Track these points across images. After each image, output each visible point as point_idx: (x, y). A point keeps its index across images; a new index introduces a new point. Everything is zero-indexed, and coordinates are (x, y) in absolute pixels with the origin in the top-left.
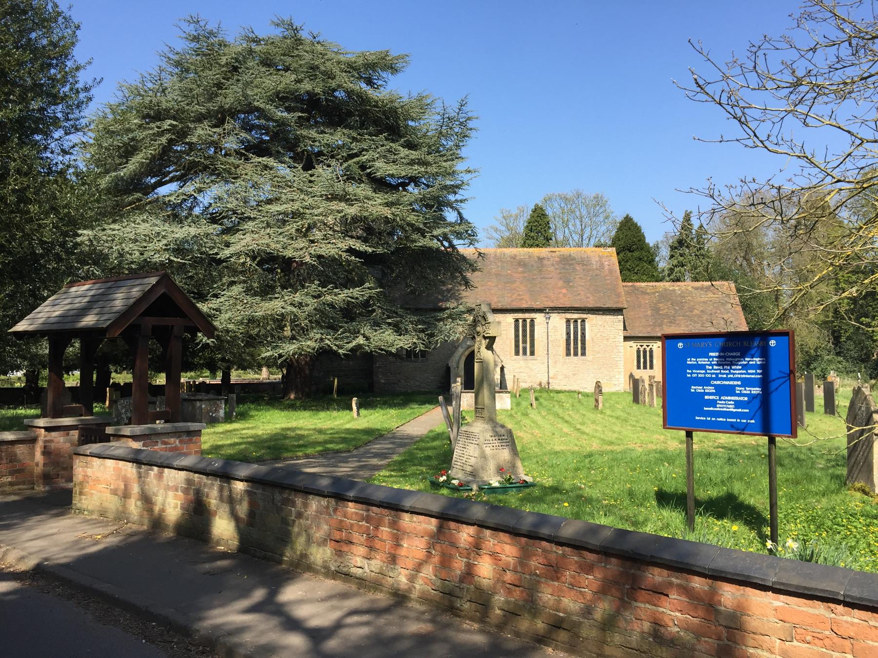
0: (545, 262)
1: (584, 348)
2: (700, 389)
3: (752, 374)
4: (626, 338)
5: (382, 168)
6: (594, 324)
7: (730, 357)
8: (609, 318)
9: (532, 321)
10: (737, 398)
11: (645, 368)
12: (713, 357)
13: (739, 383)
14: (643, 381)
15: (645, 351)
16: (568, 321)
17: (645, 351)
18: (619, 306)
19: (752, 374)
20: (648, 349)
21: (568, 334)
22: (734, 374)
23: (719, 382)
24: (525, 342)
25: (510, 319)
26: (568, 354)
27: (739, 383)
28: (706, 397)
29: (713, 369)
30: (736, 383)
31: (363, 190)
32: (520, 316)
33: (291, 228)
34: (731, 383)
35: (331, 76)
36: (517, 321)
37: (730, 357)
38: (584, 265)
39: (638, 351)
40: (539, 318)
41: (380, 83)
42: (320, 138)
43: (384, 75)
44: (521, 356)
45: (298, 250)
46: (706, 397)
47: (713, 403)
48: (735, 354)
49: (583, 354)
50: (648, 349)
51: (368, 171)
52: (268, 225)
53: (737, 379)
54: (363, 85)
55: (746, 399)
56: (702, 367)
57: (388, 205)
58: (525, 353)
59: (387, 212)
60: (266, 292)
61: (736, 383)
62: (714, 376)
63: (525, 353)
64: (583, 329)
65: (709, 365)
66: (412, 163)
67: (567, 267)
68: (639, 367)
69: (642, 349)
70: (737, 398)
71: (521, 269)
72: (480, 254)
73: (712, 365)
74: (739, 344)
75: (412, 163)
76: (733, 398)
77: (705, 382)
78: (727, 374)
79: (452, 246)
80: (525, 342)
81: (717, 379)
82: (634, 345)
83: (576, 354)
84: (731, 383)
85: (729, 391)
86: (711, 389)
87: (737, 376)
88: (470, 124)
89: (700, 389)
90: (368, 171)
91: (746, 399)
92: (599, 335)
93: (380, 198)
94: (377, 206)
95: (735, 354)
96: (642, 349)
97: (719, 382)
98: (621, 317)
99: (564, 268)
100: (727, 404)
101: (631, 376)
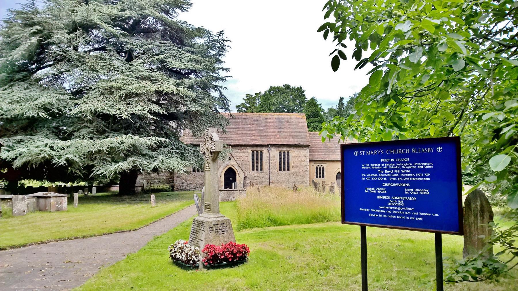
0: (268, 120)
1: (288, 167)
2: (373, 190)
3: (420, 177)
4: (310, 161)
5: (175, 64)
6: (294, 154)
7: (399, 162)
8: (301, 150)
9: (261, 153)
10: (406, 198)
11: (320, 177)
12: (385, 163)
13: (408, 185)
14: (319, 184)
15: (320, 168)
16: (280, 153)
17: (320, 168)
18: (307, 144)
19: (420, 177)
20: (322, 167)
21: (280, 159)
22: (403, 177)
23: (389, 185)
24: (257, 163)
25: (249, 151)
26: (280, 170)
27: (408, 185)
28: (378, 197)
29: (384, 173)
30: (405, 185)
31: (160, 75)
32: (255, 149)
33: (116, 95)
34: (401, 185)
35: (143, 8)
36: (253, 152)
37: (399, 162)
38: (289, 122)
39: (317, 168)
40: (265, 151)
41: (174, 14)
42: (135, 42)
43: (177, 10)
44: (255, 171)
45: (124, 111)
46: (378, 197)
47: (385, 202)
48: (404, 160)
49: (288, 170)
50: (322, 167)
51: (164, 64)
52: (102, 94)
53: (406, 182)
54: (165, 15)
55: (414, 199)
56: (375, 171)
57: (178, 85)
58: (257, 169)
59: (175, 89)
60: (102, 133)
61: (405, 185)
62: (385, 179)
63: (257, 169)
64: (288, 156)
65: (381, 170)
66: (190, 60)
67: (280, 123)
68: (317, 177)
69: (318, 167)
70: (406, 198)
71: (255, 124)
72: (231, 115)
73: (384, 170)
74: (408, 151)
75: (190, 60)
76: (402, 198)
77: (378, 184)
78: (397, 177)
79: (216, 109)
80: (257, 163)
81: (388, 181)
82: (314, 165)
83: (284, 170)
84: (401, 185)
85: (400, 191)
86: (383, 190)
87: (405, 179)
88: (226, 43)
89: (373, 190)
90: (164, 64)
91: (414, 199)
92: (296, 159)
93: (172, 81)
94: (169, 85)
95: (404, 160)
96: (318, 167)
97: (389, 185)
98: (308, 150)
99: (278, 124)
100: (397, 203)
101: (313, 181)
